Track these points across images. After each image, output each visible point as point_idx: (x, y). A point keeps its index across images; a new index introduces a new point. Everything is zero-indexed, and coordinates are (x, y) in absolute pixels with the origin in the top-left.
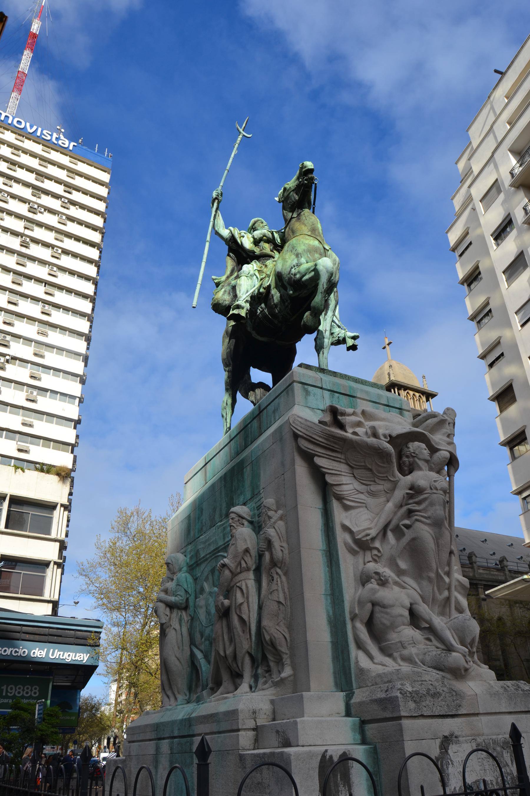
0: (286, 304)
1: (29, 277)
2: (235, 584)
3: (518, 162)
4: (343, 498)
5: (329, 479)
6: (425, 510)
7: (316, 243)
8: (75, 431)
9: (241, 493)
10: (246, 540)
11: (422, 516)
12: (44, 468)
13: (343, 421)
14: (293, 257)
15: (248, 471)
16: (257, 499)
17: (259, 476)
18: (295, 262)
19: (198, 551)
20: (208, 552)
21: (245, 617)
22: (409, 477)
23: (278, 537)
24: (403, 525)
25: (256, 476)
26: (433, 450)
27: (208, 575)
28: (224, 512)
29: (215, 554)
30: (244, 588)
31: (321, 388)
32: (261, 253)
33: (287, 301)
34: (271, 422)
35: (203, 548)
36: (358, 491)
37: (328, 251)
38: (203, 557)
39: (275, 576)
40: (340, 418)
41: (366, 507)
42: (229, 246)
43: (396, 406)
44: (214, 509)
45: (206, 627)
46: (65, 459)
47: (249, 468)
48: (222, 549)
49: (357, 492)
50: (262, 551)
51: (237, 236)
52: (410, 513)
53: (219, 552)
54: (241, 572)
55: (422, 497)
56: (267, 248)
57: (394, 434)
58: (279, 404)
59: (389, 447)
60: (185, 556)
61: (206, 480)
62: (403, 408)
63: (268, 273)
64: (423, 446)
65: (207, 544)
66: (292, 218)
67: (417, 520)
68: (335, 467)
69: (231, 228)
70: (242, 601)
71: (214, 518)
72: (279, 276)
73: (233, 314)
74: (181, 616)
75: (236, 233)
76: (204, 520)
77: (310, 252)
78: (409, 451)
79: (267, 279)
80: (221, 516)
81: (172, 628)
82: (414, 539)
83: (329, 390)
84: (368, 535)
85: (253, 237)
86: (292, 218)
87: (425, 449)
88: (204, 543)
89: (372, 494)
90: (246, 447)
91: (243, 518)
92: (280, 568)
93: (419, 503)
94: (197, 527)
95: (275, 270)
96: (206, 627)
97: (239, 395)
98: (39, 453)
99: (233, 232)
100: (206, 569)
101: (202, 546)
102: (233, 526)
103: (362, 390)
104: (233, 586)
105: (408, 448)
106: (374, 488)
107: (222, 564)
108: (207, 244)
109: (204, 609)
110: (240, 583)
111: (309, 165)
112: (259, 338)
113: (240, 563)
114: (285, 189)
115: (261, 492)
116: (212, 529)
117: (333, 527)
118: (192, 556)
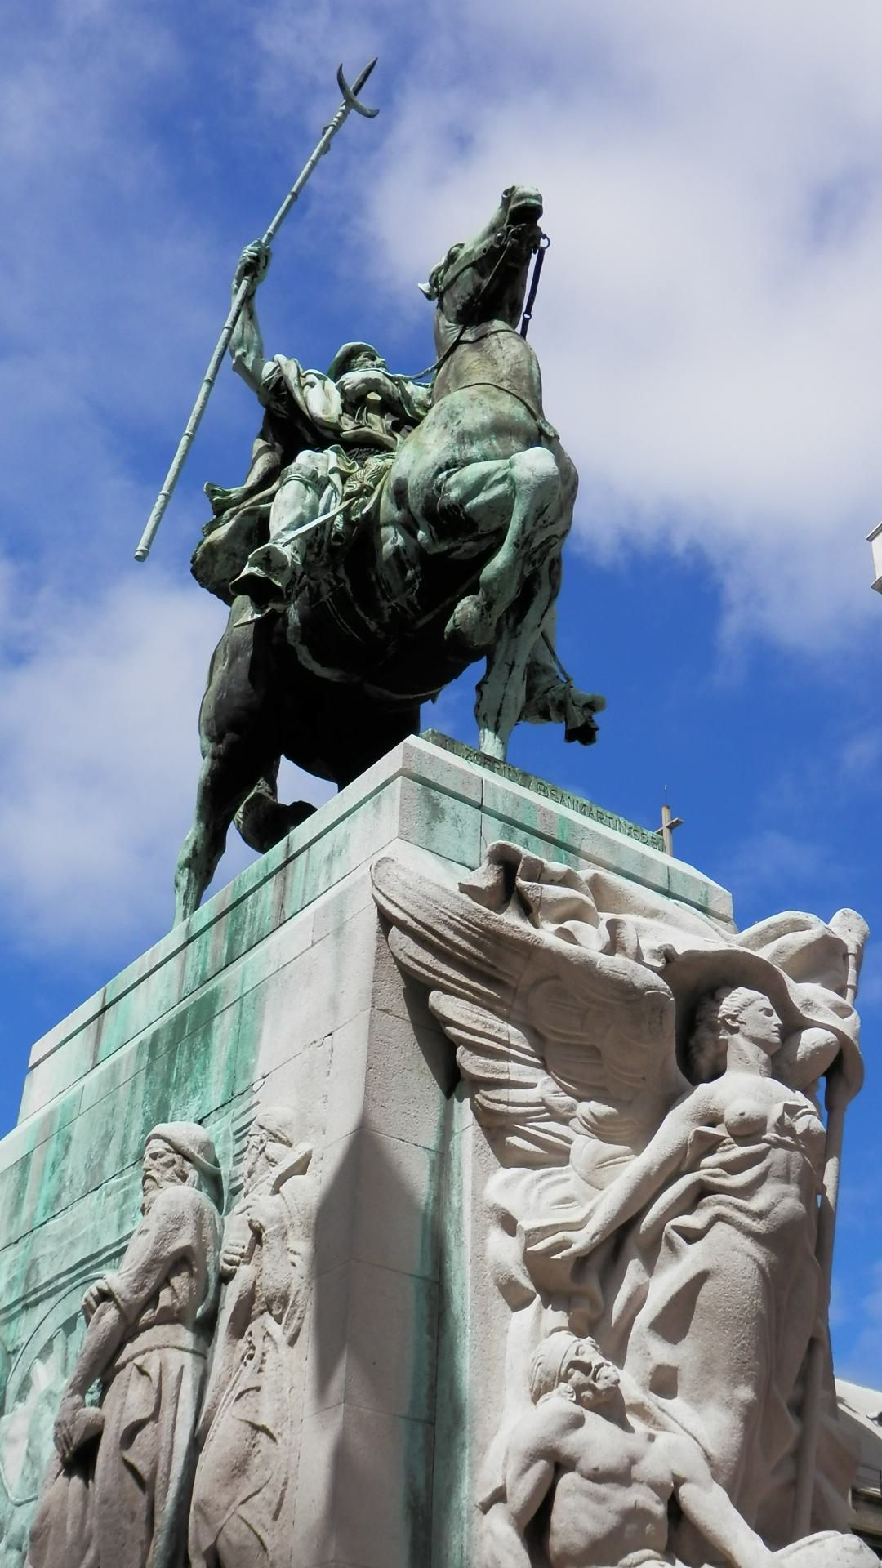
0: (409, 574)
5: (469, 1062)
9: (195, 1091)
11: (739, 1208)
15: (224, 1026)
16: (242, 1109)
17: (256, 1038)
19: (34, 1264)
24: (675, 1228)
25: (246, 1039)
27: (51, 1339)
28: (133, 1147)
30: (153, 1371)
31: (480, 807)
32: (356, 436)
34: (316, 886)
35: (53, 1255)
38: (48, 1283)
42: (267, 407)
43: (690, 897)
45: (19, 1505)
47: (228, 1014)
50: (231, 1263)
51: (293, 381)
58: (347, 836)
61: (95, 1057)
65: (66, 1242)
66: (458, 342)
67: (719, 1218)
68: (491, 1027)
71: (100, 1165)
73: (250, 576)
75: (291, 370)
76: (69, 1172)
80: (122, 1158)
83: (501, 818)
85: (343, 393)
86: (458, 342)
88: (60, 1239)
91: (187, 1157)
93: (733, 1167)
94: (45, 1192)
96: (19, 1505)
100: (49, 1320)
101: (50, 1248)
102: (153, 1179)
103: (596, 836)
107: (99, 1290)
109: (23, 1446)
115: (255, 1088)
116: (89, 1197)
118: (14, 1278)
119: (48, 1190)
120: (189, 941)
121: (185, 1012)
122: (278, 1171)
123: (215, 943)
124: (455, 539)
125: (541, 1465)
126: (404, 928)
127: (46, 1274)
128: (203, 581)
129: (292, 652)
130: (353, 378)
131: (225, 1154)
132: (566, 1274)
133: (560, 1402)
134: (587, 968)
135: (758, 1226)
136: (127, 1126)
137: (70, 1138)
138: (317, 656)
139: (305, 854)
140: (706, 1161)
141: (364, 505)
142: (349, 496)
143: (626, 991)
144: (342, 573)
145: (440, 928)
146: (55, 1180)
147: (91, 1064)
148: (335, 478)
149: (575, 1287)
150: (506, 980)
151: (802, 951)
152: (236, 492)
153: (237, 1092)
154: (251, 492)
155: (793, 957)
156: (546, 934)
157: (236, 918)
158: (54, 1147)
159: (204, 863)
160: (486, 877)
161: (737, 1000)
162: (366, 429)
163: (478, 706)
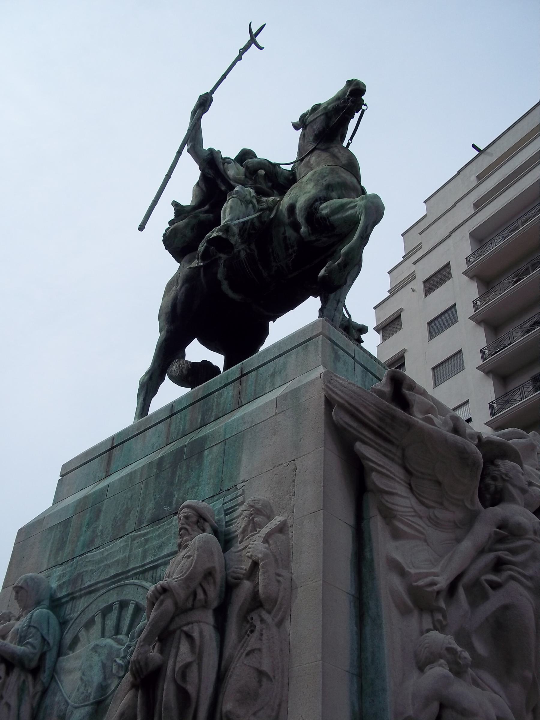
0: (290, 251)
2: (180, 628)
4: (395, 517)
6: (524, 565)
10: (212, 554)
11: (519, 573)
19: (80, 576)
20: (103, 578)
21: (191, 689)
22: (497, 509)
29: (119, 581)
30: (196, 635)
31: (353, 358)
33: (293, 247)
36: (415, 511)
39: (258, 624)
41: (425, 541)
45: (76, 708)
47: (215, 449)
48: (136, 574)
49: (413, 514)
50: (236, 578)
52: (499, 565)
53: (127, 578)
54: (193, 608)
55: (519, 543)
58: (285, 364)
61: (107, 472)
67: (512, 578)
70: (189, 659)
74: (24, 682)
76: (100, 528)
78: (499, 471)
81: (4, 701)
82: (505, 608)
84: (433, 584)
89: (436, 523)
90: (203, 425)
92: (269, 612)
93: (514, 552)
94: (82, 538)
96: (76, 708)
104: (174, 631)
105: (497, 466)
106: (440, 513)
110: (190, 626)
112: (230, 293)
113: (195, 594)
115: (238, 487)
117: (372, 560)
120: (172, 415)
121: (182, 448)
125: (435, 707)
126: (341, 406)
129: (219, 283)
133: (439, 670)
137: (100, 511)
138: (232, 286)
139: (255, 372)
143: (463, 455)
144: (253, 246)
145: (362, 409)
148: (255, 201)
150: (394, 440)
153: (224, 489)
157: (109, 454)
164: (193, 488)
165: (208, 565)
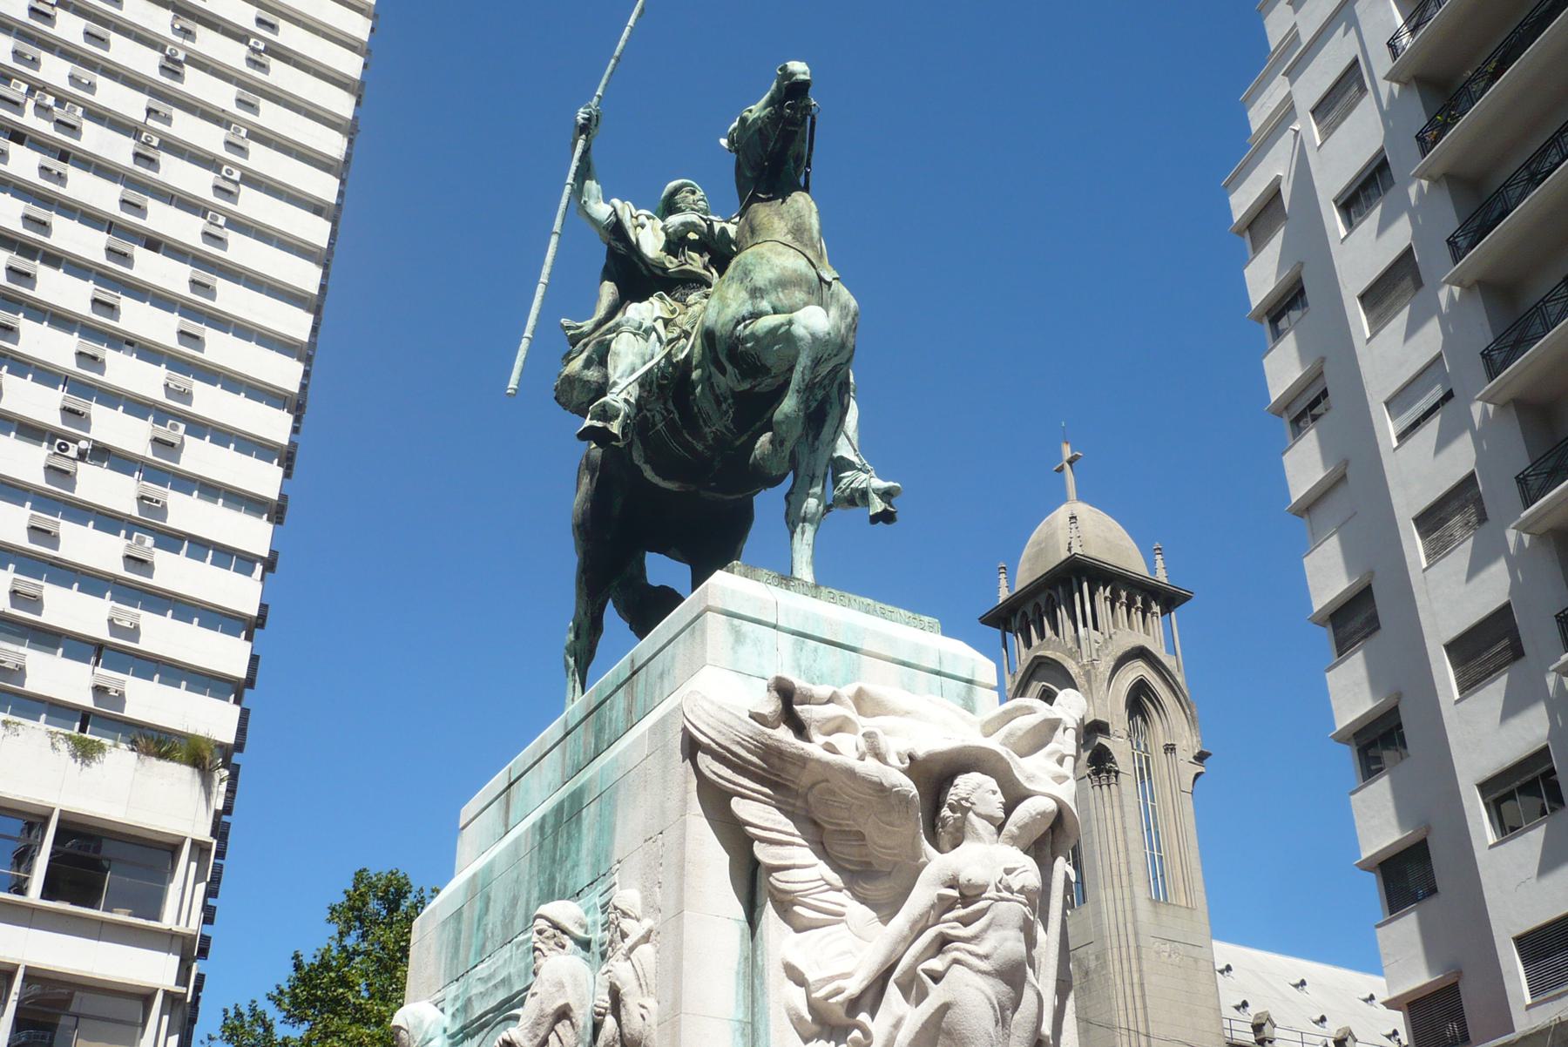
0: (724, 406)
1: (153, 243)
3: (1407, 22)
5: (762, 853)
7: (801, 264)
8: (249, 645)
11: (970, 953)
12: (156, 742)
13: (803, 716)
14: (744, 295)
15: (589, 814)
18: (747, 308)
23: (635, 983)
24: (924, 971)
25: (607, 829)
26: (1014, 795)
31: (775, 627)
33: (726, 399)
37: (829, 284)
40: (797, 708)
44: (514, 902)
46: (215, 720)
50: (599, 1014)
51: (628, 223)
56: (696, 262)
57: (920, 753)
59: (908, 786)
60: (442, 1010)
61: (506, 825)
62: (977, 678)
63: (688, 327)
64: (991, 783)
67: (956, 961)
69: (616, 202)
72: (709, 336)
75: (626, 210)
77: (787, 279)
79: (683, 341)
82: (945, 1008)
83: (794, 633)
84: (838, 992)
85: (664, 229)
87: (994, 793)
93: (966, 922)
95: (703, 323)
97: (611, 615)
98: (149, 701)
99: (620, 213)
108: (554, 240)
111: (799, 68)
114: (743, 120)
119: (476, 943)
120: (567, 734)
122: (629, 942)
123: (584, 736)
124: (755, 378)
126: (708, 750)
127: (478, 1010)
128: (565, 406)
130: (675, 220)
131: (595, 923)
132: (841, 1012)
134: (850, 773)
135: (984, 965)
136: (529, 892)
140: (946, 916)
141: (684, 348)
142: (670, 341)
144: (671, 406)
146: (481, 934)
147: (502, 831)
148: (659, 325)
149: (850, 1021)
151: (1028, 732)
152: (588, 325)
154: (599, 324)
155: (1021, 738)
156: (814, 748)
157: (599, 718)
158: (478, 904)
159: (584, 655)
160: (770, 705)
161: (966, 785)
162: (687, 267)
163: (787, 514)
164: (573, 868)
165: (561, 1002)
